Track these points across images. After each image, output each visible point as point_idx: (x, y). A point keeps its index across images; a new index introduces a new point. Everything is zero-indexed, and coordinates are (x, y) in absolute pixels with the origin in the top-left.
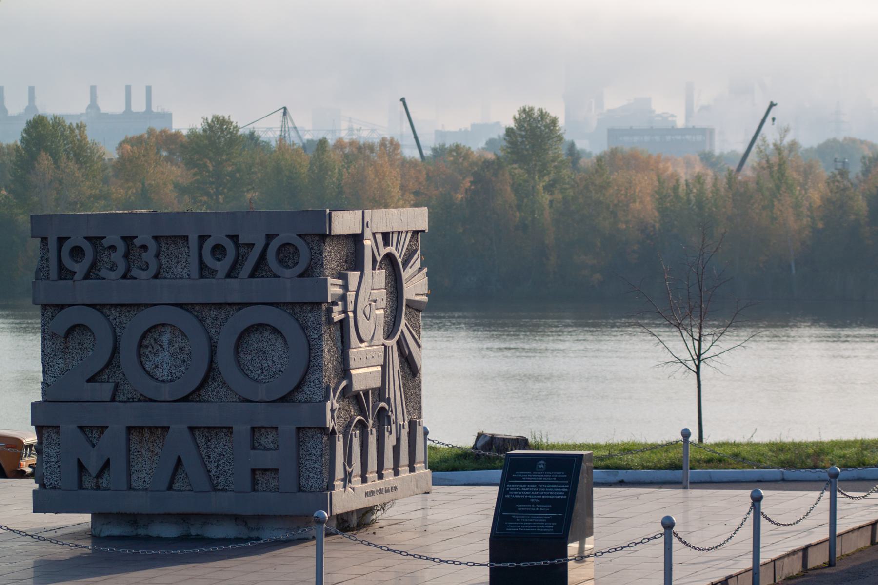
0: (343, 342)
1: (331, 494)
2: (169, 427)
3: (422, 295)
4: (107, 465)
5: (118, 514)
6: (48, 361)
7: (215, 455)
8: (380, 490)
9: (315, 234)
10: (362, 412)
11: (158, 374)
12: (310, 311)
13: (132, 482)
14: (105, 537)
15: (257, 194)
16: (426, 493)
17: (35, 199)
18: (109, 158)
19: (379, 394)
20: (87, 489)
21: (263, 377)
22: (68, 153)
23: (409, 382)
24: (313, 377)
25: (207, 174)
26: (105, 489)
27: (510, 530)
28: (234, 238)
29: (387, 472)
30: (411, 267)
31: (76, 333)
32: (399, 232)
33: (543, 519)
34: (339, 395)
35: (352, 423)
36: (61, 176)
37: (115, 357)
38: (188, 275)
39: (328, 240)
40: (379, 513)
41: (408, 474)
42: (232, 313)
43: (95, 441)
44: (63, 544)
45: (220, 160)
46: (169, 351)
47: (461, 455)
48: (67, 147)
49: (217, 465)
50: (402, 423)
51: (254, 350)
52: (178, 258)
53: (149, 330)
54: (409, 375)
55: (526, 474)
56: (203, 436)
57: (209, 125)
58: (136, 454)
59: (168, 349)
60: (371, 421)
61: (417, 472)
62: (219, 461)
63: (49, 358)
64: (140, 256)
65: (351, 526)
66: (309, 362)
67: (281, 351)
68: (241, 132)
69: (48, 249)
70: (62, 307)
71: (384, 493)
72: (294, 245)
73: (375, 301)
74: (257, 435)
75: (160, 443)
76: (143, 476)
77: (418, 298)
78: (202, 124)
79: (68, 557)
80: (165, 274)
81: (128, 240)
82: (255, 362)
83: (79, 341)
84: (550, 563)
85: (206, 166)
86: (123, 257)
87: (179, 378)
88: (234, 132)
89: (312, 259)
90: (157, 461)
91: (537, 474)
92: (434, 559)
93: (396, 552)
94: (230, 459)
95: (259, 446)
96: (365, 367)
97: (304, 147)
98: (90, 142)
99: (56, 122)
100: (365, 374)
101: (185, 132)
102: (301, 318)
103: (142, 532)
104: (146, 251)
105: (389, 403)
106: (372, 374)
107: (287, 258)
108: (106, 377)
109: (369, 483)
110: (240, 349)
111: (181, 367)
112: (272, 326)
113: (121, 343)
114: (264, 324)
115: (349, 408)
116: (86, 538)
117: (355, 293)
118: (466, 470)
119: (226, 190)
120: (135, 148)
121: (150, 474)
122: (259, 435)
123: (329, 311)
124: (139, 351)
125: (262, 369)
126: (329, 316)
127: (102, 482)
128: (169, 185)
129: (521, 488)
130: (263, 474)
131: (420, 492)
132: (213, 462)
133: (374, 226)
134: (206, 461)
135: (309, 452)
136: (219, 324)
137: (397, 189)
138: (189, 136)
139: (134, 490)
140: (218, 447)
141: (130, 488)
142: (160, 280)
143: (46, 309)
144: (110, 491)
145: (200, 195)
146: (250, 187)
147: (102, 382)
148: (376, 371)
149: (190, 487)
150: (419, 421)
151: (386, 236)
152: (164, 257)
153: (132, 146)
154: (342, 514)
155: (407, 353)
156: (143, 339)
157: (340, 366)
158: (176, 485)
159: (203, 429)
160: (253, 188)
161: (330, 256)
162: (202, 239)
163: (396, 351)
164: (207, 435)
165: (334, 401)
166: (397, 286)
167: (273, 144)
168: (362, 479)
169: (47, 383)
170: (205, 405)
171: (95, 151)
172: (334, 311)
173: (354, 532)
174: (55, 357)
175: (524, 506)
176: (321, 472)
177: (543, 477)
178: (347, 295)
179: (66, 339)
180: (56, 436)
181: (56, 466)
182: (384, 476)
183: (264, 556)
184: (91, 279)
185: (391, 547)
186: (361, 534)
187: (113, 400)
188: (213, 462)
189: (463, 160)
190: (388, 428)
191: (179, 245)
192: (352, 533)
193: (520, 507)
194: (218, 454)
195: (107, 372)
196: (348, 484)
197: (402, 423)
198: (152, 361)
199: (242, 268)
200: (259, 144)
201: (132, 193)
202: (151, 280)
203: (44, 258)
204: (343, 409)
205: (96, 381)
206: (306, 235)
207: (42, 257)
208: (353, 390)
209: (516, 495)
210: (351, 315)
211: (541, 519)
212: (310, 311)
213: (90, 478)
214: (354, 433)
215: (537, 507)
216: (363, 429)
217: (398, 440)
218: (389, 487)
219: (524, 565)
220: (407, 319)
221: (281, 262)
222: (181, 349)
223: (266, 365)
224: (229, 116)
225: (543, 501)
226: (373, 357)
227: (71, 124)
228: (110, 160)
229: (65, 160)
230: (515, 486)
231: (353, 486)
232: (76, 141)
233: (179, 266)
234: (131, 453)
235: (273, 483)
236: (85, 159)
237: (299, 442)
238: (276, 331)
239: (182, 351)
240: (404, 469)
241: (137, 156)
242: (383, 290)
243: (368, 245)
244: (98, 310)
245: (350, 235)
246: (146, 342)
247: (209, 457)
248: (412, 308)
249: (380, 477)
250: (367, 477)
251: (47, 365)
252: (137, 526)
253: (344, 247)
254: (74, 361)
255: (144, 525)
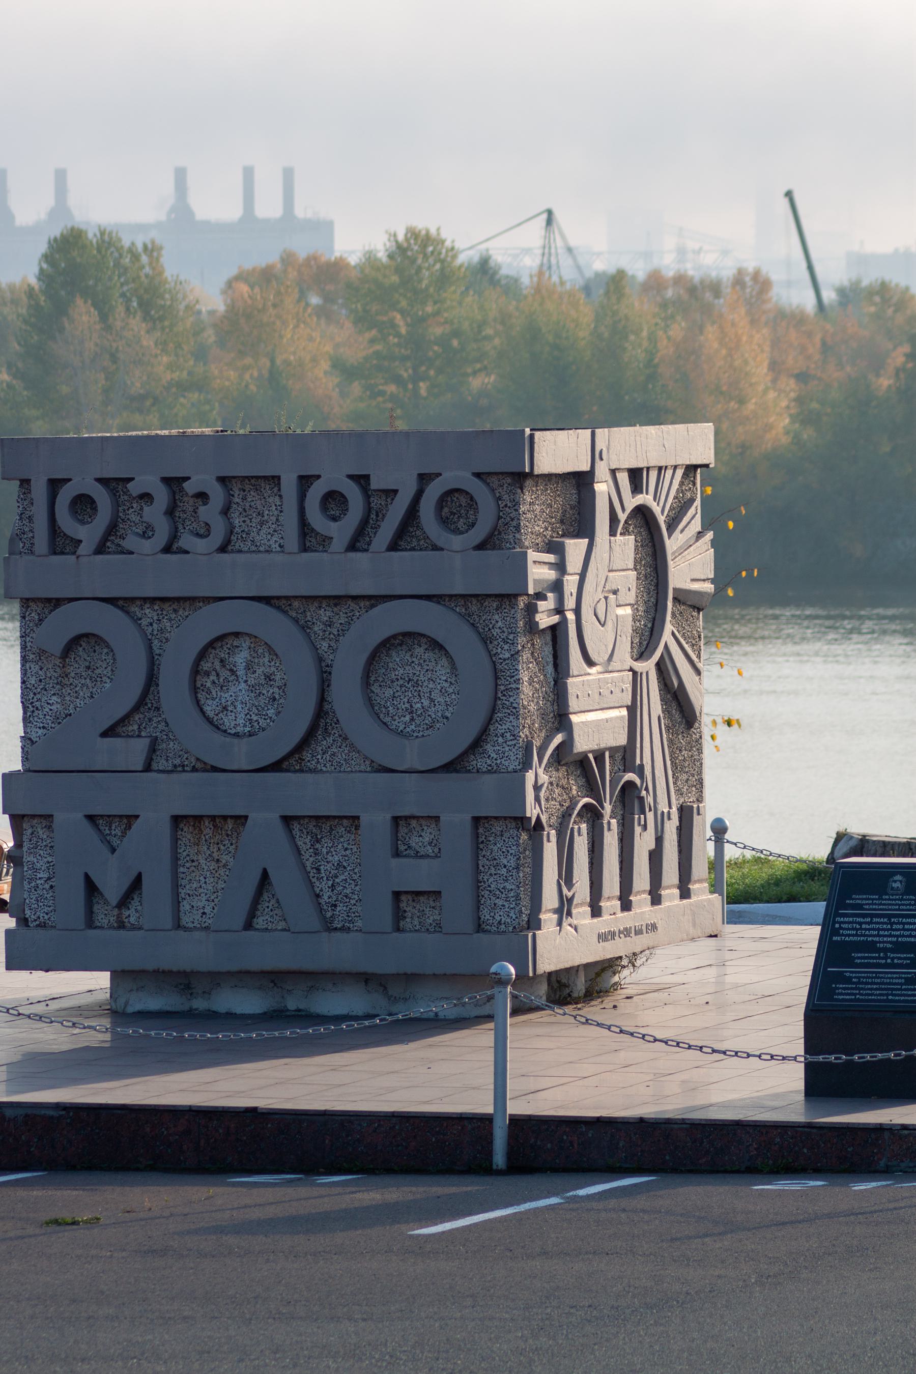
0: (556, 666)
1: (534, 936)
2: (246, 817)
3: (704, 580)
4: (137, 883)
5: (156, 972)
6: (33, 698)
7: (329, 866)
8: (626, 929)
9: (506, 473)
10: (592, 790)
11: (228, 721)
12: (497, 609)
13: (181, 914)
14: (134, 1013)
15: (493, 378)
16: (711, 936)
17: (65, 389)
18: (209, 308)
19: (624, 758)
20: (101, 928)
21: (413, 727)
22: (129, 300)
23: (680, 736)
24: (501, 729)
25: (396, 340)
26: (134, 928)
27: (841, 997)
28: (362, 480)
29: (638, 897)
30: (682, 531)
31: (81, 649)
32: (660, 468)
33: (900, 978)
34: (549, 760)
35: (574, 809)
36: (114, 345)
37: (151, 692)
38: (280, 546)
39: (529, 483)
40: (626, 972)
41: (677, 901)
42: (358, 614)
43: (115, 842)
44: (52, 1022)
45: (420, 313)
46: (246, 681)
47: (806, 873)
48: (125, 288)
49: (333, 885)
50: (666, 810)
51: (398, 680)
52: (263, 516)
53: (211, 645)
54: (680, 723)
55: (868, 899)
56: (308, 833)
57: (399, 246)
58: (188, 865)
59: (245, 678)
60: (608, 808)
61: (694, 899)
62: (337, 877)
63: (35, 694)
64: (196, 513)
65: (575, 995)
66: (495, 701)
67: (446, 681)
68: (462, 259)
69: (32, 499)
70: (56, 603)
71: (633, 934)
72: (467, 493)
73: (615, 592)
74: (403, 831)
75: (232, 844)
76: (201, 904)
77: (696, 586)
78: (385, 245)
79: (65, 1048)
80: (239, 545)
81: (174, 483)
82: (398, 699)
83: (88, 664)
84: (906, 1056)
85: (393, 325)
86: (166, 513)
87: (264, 730)
88: (449, 259)
89: (499, 518)
90: (225, 878)
91: (889, 899)
92: (701, 1048)
93: (635, 1034)
94: (355, 873)
95: (406, 850)
96: (596, 710)
97: (587, 289)
98: (169, 279)
99: (103, 241)
100: (597, 723)
101: (353, 260)
102: (481, 622)
103: (199, 1004)
104: (205, 504)
105: (641, 775)
106: (609, 722)
107: (456, 516)
108: (136, 727)
109: (606, 917)
110: (373, 678)
111: (268, 709)
112: (429, 637)
113: (161, 667)
114: (415, 633)
115: (569, 783)
116: (101, 1016)
117: (578, 577)
118: (813, 900)
119: (432, 373)
120: (257, 290)
121: (213, 901)
122: (406, 831)
123: (531, 610)
124: (193, 681)
125: (412, 712)
126: (530, 620)
127: (129, 916)
128: (322, 362)
129: (860, 924)
130: (414, 901)
131: (700, 935)
132: (325, 879)
133: (613, 457)
134: (313, 877)
135: (495, 862)
136: (336, 633)
137: (764, 369)
138: (360, 267)
139: (186, 929)
140: (334, 853)
141: (178, 926)
142: (231, 555)
143: (28, 607)
144: (142, 931)
145: (382, 381)
146: (478, 366)
147: (128, 736)
148: (617, 718)
149: (284, 923)
150: (698, 806)
151: (636, 475)
152: (237, 514)
153: (252, 287)
154: (557, 972)
155: (676, 684)
156: (200, 661)
157: (550, 709)
158: (260, 920)
159: (306, 820)
160: (485, 368)
161: (533, 511)
162: (305, 481)
163: (656, 681)
164: (314, 830)
165: (541, 771)
166: (656, 565)
167: (526, 281)
168: (592, 911)
169: (30, 739)
170: (309, 777)
171: (180, 296)
172: (540, 609)
173: (579, 1006)
174: (45, 693)
175: (866, 955)
176: (517, 897)
177: (899, 905)
178: (563, 580)
179: (65, 661)
180: (48, 833)
181: (47, 886)
182: (633, 904)
183: (412, 1045)
184: (109, 553)
185: (722, 1056)
186: (591, 1008)
187: (148, 768)
188: (325, 879)
189: (896, 311)
190: (639, 818)
191: (264, 491)
192: (575, 1006)
193: (859, 958)
194: (333, 865)
195: (137, 719)
196: (567, 918)
197: (666, 810)
198: (217, 700)
199: (375, 533)
200: (499, 281)
201: (251, 376)
202: (215, 554)
203: (25, 516)
204: (557, 785)
205: (118, 736)
206: (489, 474)
207: (21, 514)
208: (575, 751)
209: (853, 935)
210: (571, 616)
211: (896, 978)
212: (497, 609)
213: (106, 908)
214: (576, 827)
215: (889, 958)
216: (594, 821)
217: (659, 840)
218: (642, 925)
219: (859, 1058)
220: (678, 625)
221: (445, 522)
222: (269, 678)
223: (419, 705)
224: (438, 229)
225: (899, 947)
226: (612, 692)
227: (133, 244)
228: (212, 313)
229: (122, 314)
230: (851, 919)
231: (574, 922)
232: (143, 278)
233: (265, 529)
234: (179, 863)
235: (432, 917)
236: (161, 313)
237: (478, 844)
238: (436, 645)
239: (270, 680)
240: (670, 893)
241: (260, 306)
242: (630, 572)
243: (602, 493)
244: (121, 608)
245: (569, 474)
246: (205, 666)
247: (318, 870)
248: (684, 604)
249: (626, 906)
250: (601, 906)
251: (30, 706)
252: (191, 994)
253: (559, 495)
254: (78, 700)
255: (204, 992)
